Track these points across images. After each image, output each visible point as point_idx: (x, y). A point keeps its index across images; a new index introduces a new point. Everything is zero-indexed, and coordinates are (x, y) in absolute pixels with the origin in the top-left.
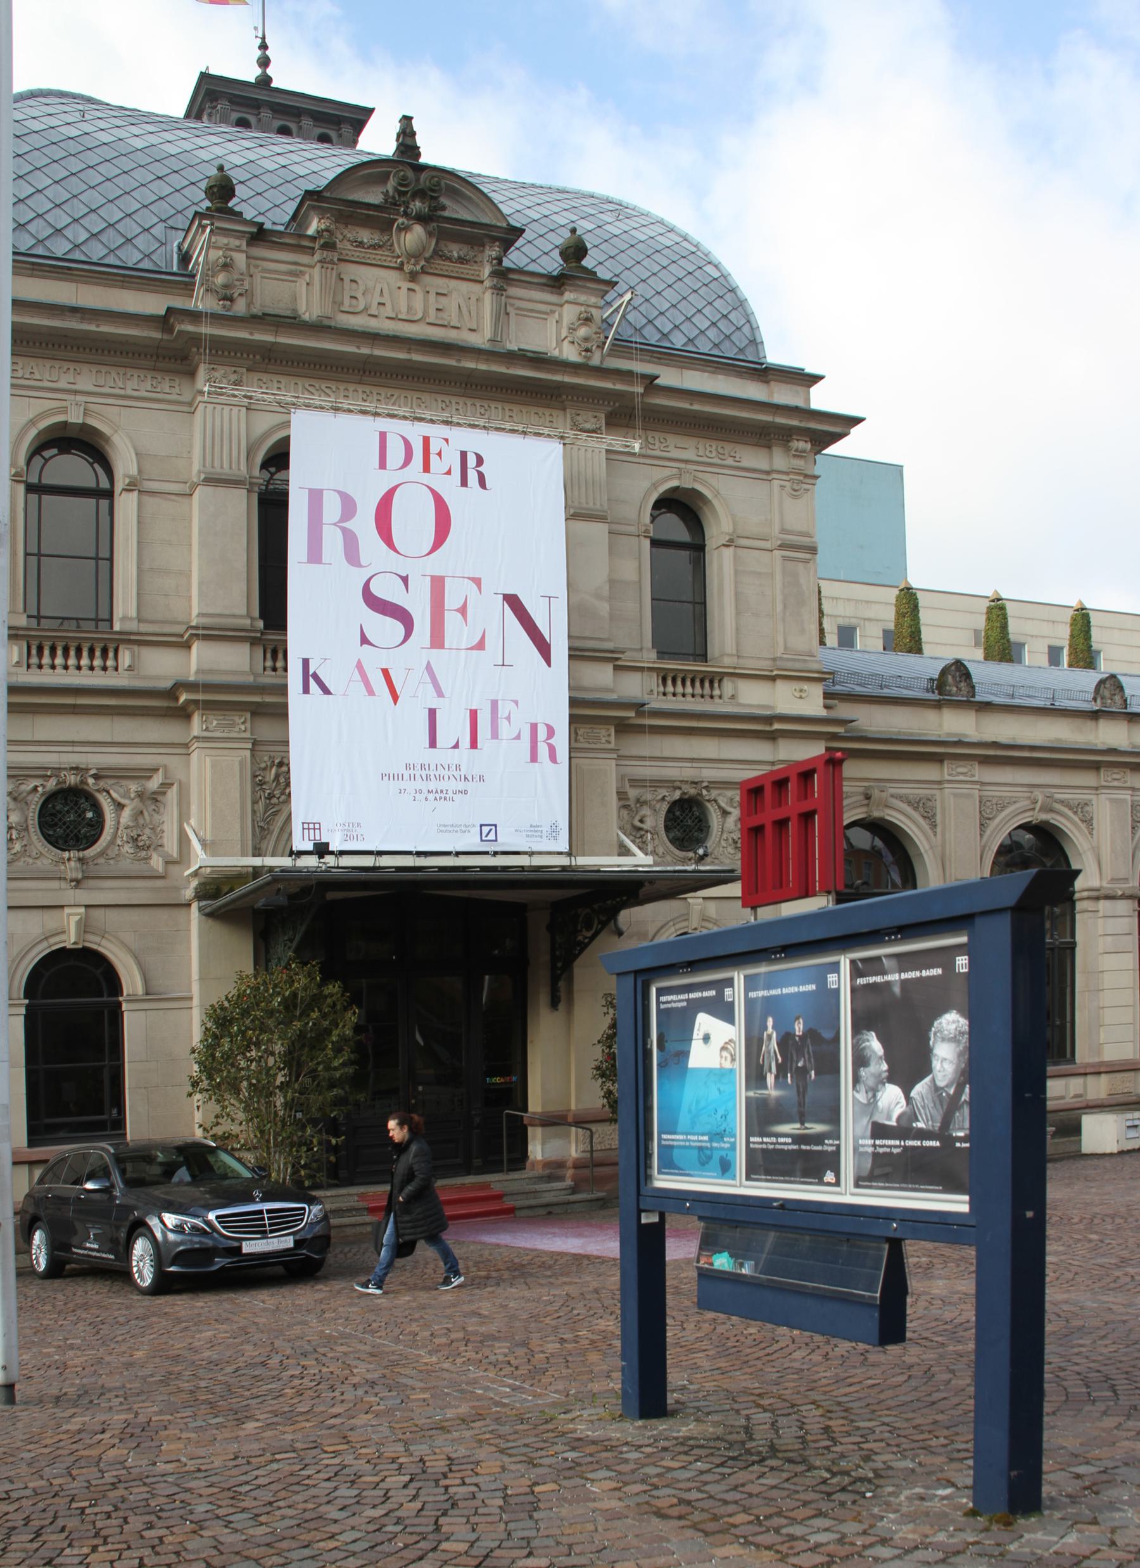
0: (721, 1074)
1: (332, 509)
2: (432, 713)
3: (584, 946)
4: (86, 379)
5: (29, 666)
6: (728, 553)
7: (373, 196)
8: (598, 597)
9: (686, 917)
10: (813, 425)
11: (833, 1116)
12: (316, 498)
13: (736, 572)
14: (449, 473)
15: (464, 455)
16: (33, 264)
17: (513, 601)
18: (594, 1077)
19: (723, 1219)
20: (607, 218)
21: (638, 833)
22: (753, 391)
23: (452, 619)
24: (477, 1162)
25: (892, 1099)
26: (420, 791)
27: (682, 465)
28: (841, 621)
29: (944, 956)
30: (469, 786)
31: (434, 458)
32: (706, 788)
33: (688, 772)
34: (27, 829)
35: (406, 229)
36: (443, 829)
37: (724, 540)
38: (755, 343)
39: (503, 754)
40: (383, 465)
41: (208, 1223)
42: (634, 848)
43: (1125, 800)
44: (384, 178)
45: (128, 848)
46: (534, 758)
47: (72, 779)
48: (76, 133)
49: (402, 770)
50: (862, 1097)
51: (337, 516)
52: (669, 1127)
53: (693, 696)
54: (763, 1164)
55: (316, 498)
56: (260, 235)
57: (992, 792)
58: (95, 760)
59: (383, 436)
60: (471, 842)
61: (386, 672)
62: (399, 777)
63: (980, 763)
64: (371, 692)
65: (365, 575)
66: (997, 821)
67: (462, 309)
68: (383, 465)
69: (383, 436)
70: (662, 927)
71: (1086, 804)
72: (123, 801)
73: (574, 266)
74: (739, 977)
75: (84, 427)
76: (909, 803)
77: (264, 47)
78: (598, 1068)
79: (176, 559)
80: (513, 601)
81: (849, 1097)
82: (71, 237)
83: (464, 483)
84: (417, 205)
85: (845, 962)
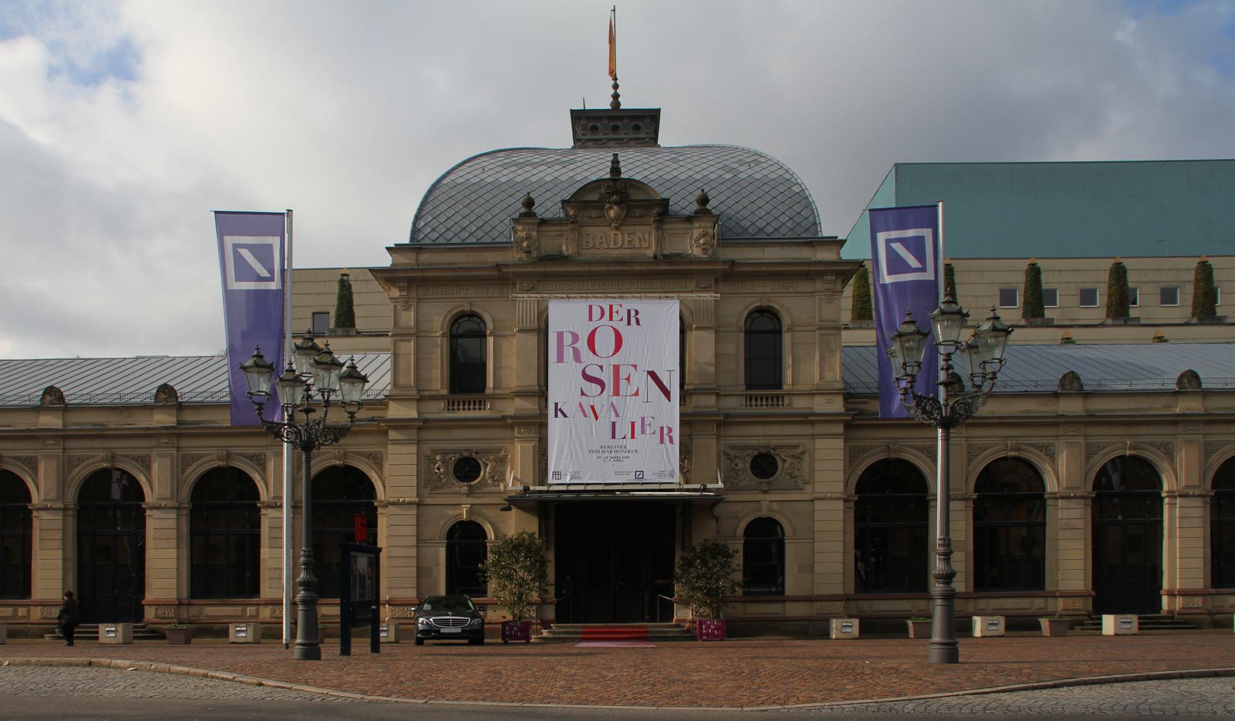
1: (568, 339)
2: (614, 424)
4: (471, 293)
7: (595, 197)
8: (709, 364)
10: (834, 268)
12: (560, 335)
15: (629, 311)
17: (652, 374)
23: (623, 383)
24: (647, 617)
33: (763, 442)
35: (611, 208)
36: (617, 473)
38: (815, 224)
39: (646, 443)
40: (591, 319)
44: (599, 187)
45: (490, 482)
46: (662, 441)
47: (466, 454)
55: (560, 335)
56: (543, 222)
58: (774, 442)
59: (591, 307)
60: (631, 478)
61: (592, 407)
62: (597, 452)
65: (583, 366)
67: (643, 241)
68: (591, 319)
69: (591, 307)
79: (506, 362)
80: (652, 374)
83: (629, 323)
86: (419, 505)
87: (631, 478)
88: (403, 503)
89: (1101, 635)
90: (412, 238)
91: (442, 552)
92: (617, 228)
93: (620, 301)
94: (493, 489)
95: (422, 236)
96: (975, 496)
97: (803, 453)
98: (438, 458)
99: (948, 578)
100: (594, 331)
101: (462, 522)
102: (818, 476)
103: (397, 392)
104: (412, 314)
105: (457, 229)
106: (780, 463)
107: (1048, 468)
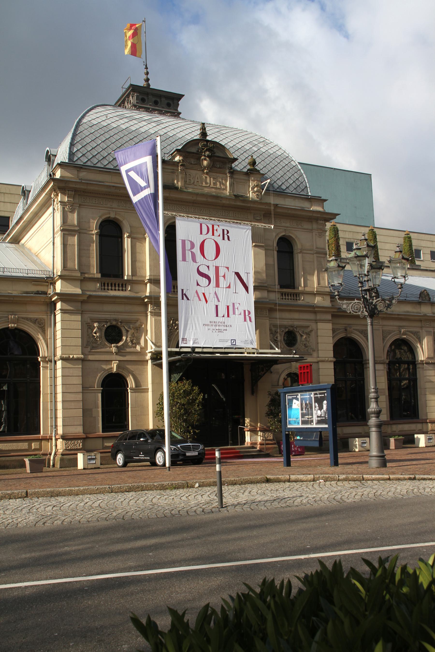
0: (297, 409)
2: (217, 306)
3: (261, 377)
5: (101, 289)
6: (300, 255)
9: (291, 367)
11: (312, 415)
13: (303, 261)
14: (219, 236)
15: (223, 230)
16: (100, 170)
17: (237, 274)
18: (266, 416)
19: (299, 431)
20: (261, 145)
21: (275, 342)
22: (305, 205)
23: (221, 279)
24: (230, 442)
25: (319, 413)
26: (214, 330)
27: (286, 228)
28: (347, 240)
29: (324, 393)
30: (227, 328)
31: (215, 231)
32: (296, 328)
33: (290, 323)
34: (101, 337)
36: (221, 341)
37: (299, 251)
39: (237, 319)
40: (201, 233)
41: (178, 448)
42: (275, 347)
43: (431, 331)
45: (130, 344)
46: (245, 320)
47: (114, 323)
48: (106, 124)
49: (209, 323)
50: (316, 412)
51: (189, 248)
52: (290, 418)
53: (291, 299)
54: (304, 422)
55: (184, 242)
57: (383, 329)
58: (296, 323)
59: (201, 225)
60: (228, 344)
61: (204, 294)
62: (208, 325)
63: (382, 319)
64: (200, 300)
66: (388, 338)
68: (201, 233)
70: (283, 371)
71: (418, 332)
72: (128, 329)
73: (253, 171)
74: (299, 394)
75: (115, 218)
76: (359, 332)
77: (147, 68)
78: (267, 413)
80: (237, 274)
81: (314, 412)
82: (108, 159)
83: (224, 239)
84: (207, 153)
85: (313, 393)
86: (83, 360)
87: (228, 344)
88: (73, 359)
89: (77, 470)
90: (70, 159)
91: (100, 395)
92: (207, 173)
93: (219, 223)
94: (132, 350)
95: (75, 159)
96: (334, 360)
97: (311, 331)
98: (96, 325)
99: (378, 413)
100: (203, 242)
101: (112, 374)
102: (321, 346)
103: (66, 273)
104: (76, 215)
105: (99, 157)
106: (299, 337)
107: (40, 337)
